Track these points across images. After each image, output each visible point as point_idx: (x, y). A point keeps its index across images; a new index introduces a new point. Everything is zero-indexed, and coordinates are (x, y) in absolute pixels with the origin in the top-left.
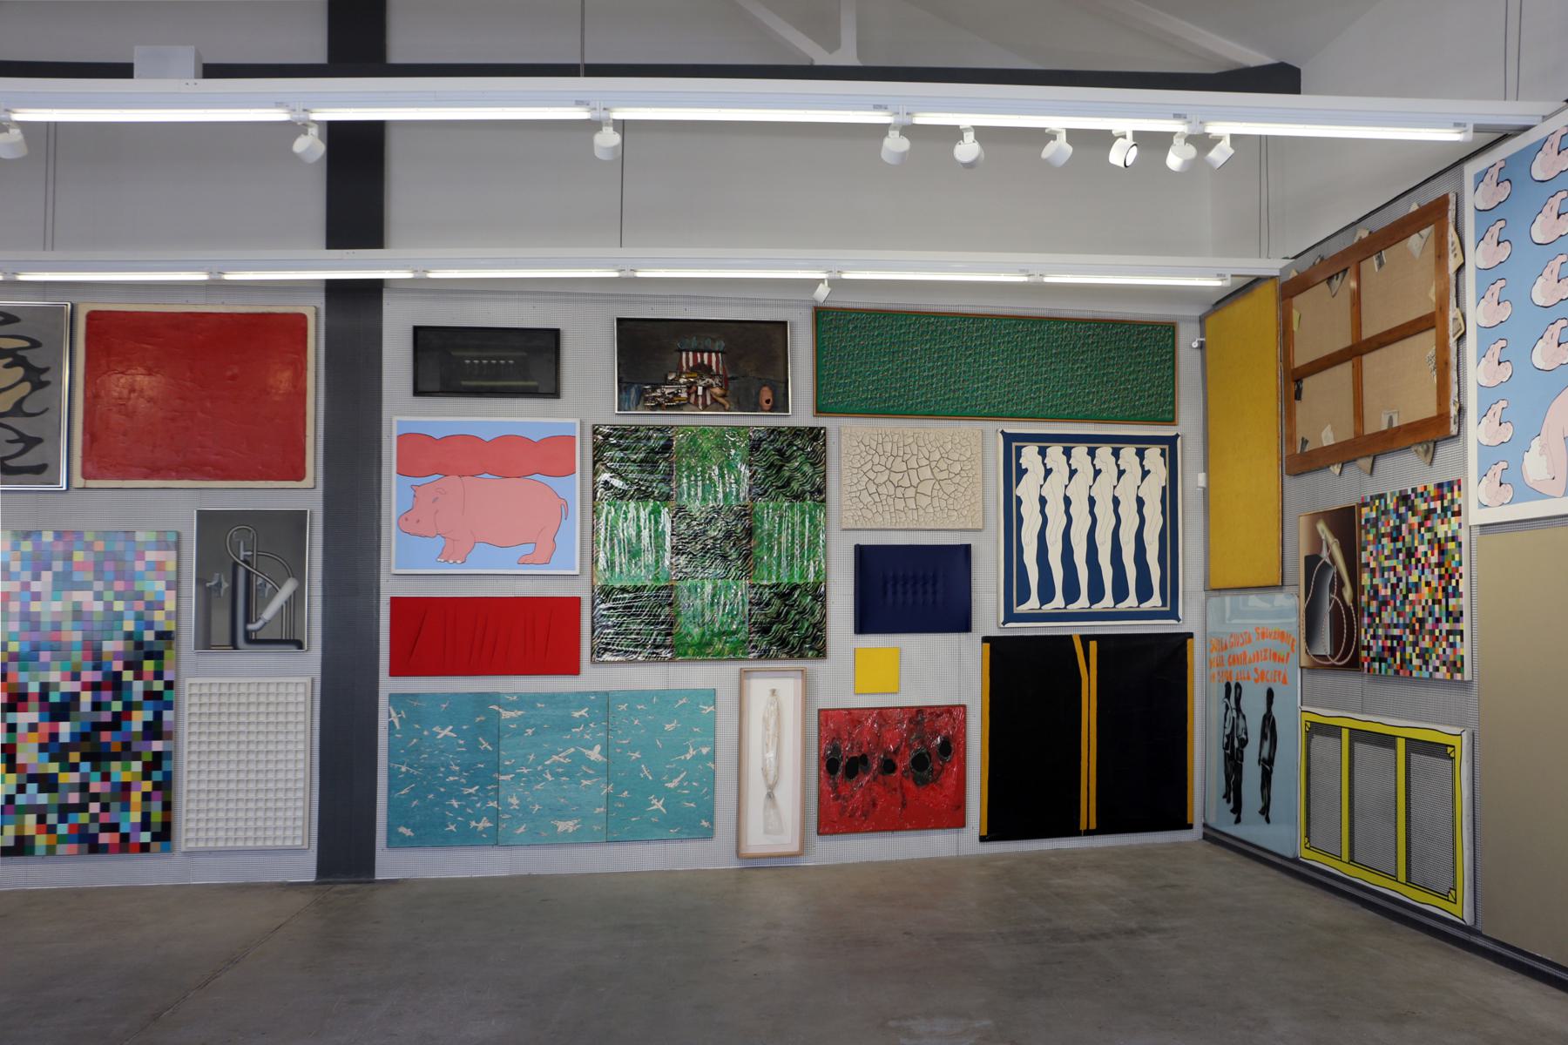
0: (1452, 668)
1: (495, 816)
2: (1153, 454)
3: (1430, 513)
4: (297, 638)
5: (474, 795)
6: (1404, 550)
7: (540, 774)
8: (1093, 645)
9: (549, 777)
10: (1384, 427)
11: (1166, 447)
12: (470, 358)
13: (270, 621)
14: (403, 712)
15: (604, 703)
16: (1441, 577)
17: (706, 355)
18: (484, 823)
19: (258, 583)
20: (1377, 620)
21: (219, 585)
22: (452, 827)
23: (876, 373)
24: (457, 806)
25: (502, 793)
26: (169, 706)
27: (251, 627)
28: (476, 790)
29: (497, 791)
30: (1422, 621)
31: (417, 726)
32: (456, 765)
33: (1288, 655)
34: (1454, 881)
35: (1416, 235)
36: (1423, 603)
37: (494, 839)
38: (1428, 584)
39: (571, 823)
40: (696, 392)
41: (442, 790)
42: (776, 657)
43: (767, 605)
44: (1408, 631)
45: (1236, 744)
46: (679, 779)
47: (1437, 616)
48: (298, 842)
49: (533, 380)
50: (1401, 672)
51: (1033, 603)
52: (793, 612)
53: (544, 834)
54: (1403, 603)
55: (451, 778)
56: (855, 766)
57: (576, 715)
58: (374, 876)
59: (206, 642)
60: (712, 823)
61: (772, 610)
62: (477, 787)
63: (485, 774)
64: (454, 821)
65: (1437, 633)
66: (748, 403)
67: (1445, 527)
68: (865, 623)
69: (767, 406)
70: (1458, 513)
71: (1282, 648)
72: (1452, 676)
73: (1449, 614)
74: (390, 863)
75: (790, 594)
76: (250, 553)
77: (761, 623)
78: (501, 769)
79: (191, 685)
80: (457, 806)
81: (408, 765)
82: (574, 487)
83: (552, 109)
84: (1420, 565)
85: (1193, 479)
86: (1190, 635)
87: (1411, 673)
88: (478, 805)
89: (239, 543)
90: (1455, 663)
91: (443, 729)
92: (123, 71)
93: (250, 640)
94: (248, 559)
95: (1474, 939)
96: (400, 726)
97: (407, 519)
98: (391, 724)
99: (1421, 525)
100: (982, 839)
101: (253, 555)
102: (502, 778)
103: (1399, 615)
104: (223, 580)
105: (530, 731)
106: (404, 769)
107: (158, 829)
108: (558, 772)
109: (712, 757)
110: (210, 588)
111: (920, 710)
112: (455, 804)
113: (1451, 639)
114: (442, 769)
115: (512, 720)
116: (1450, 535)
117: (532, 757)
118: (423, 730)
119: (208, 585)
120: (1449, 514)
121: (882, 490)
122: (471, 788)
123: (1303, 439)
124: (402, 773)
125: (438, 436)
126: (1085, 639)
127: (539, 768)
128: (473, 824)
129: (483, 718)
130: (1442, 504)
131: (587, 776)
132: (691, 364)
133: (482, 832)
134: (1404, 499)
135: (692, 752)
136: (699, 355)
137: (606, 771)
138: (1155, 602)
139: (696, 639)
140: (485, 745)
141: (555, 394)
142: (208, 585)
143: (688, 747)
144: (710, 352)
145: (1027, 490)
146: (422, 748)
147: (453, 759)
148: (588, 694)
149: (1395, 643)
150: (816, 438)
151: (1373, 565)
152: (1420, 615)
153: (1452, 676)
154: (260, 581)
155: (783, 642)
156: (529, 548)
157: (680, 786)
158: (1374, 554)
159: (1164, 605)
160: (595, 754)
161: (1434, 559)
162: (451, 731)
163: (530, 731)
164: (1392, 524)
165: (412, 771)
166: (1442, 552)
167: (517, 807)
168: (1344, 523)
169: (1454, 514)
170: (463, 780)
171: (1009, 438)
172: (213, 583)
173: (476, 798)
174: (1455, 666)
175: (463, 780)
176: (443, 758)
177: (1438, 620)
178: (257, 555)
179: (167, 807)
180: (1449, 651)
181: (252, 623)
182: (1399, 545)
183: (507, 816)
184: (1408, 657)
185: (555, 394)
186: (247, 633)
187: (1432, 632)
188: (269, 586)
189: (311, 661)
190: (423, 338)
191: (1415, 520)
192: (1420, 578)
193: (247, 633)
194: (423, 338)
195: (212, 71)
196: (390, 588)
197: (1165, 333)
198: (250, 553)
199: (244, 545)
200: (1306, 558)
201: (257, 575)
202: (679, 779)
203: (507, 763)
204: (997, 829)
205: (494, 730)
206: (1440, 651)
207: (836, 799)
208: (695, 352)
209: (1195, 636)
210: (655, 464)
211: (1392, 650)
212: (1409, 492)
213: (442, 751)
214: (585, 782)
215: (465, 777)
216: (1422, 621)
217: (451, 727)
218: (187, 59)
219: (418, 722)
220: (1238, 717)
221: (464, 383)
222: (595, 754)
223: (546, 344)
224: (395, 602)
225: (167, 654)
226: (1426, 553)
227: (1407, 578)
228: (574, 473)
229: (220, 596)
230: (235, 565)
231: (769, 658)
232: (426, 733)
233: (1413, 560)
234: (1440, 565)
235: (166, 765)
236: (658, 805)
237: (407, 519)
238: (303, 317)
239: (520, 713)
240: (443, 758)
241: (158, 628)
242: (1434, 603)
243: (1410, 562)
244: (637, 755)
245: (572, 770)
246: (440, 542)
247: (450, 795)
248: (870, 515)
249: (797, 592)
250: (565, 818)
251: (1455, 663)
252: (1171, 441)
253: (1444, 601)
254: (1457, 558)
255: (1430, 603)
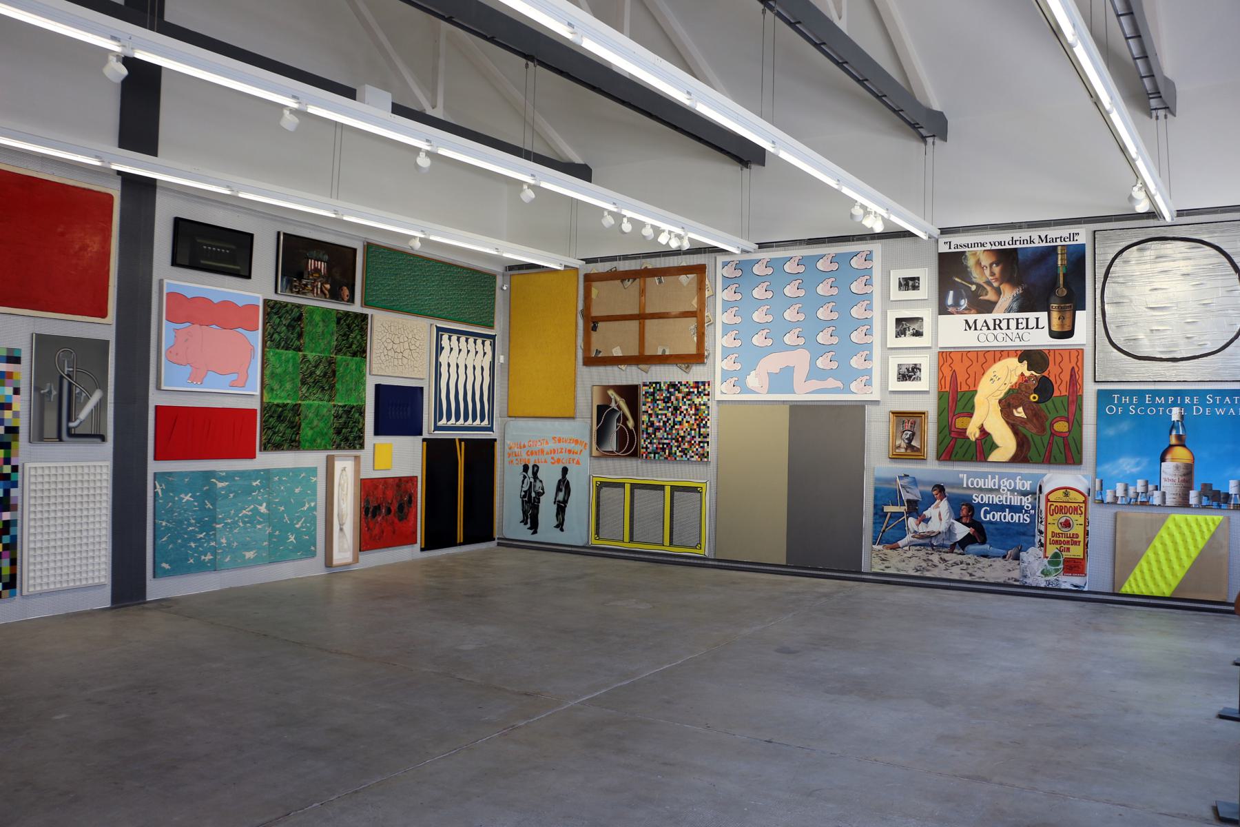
0: (701, 457)
1: (214, 551)
2: (488, 343)
3: (689, 393)
4: (101, 433)
5: (203, 539)
6: (672, 407)
7: (235, 523)
8: (463, 443)
9: (241, 524)
10: (660, 353)
11: (492, 340)
12: (208, 245)
13: (84, 420)
14: (163, 485)
15: (267, 475)
16: (696, 420)
17: (319, 263)
18: (209, 557)
19: (77, 392)
20: (653, 436)
21: (50, 392)
22: (192, 561)
23: (389, 285)
24: (194, 547)
25: (218, 536)
26: (15, 485)
27: (72, 425)
28: (204, 535)
29: (214, 534)
30: (683, 438)
31: (171, 494)
32: (193, 519)
33: (581, 451)
34: (700, 540)
35: (684, 276)
36: (684, 430)
37: (214, 567)
38: (688, 422)
39: (252, 553)
40: (317, 286)
41: (186, 536)
42: (344, 449)
43: (341, 417)
44: (674, 441)
45: (533, 495)
46: (301, 522)
47: (693, 435)
48: (103, 580)
49: (238, 266)
50: (669, 458)
51: (444, 422)
52: (351, 422)
53: (239, 561)
54: (671, 429)
55: (191, 528)
56: (377, 509)
57: (254, 484)
58: (145, 599)
59: (39, 436)
60: (316, 548)
61: (341, 421)
62: (204, 533)
63: (208, 524)
64: (192, 556)
65: (693, 442)
66: (335, 295)
67: (700, 400)
68: (378, 432)
69: (346, 298)
70: (708, 395)
71: (577, 448)
72: (701, 460)
73: (700, 435)
74: (156, 589)
75: (350, 412)
76: (71, 369)
77: (338, 428)
78: (217, 521)
79: (30, 468)
80: (194, 547)
81: (168, 521)
82: (257, 337)
83: (339, 115)
84: (683, 414)
85: (501, 359)
86: (495, 440)
87: (675, 459)
88: (205, 545)
89: (64, 361)
90: (703, 454)
91: (186, 496)
92: (350, 93)
93: (71, 434)
94: (71, 374)
95: (707, 562)
96: (162, 494)
97: (170, 352)
98: (155, 494)
99: (683, 398)
100: (422, 550)
101: (73, 371)
102: (218, 526)
103: (668, 434)
104: (53, 389)
105: (232, 495)
106: (164, 524)
107: (7, 580)
108: (245, 521)
109: (315, 508)
110: (43, 394)
111: (400, 479)
112: (193, 545)
113: (701, 445)
114: (186, 523)
115: (223, 488)
116: (702, 403)
117: (233, 512)
118: (175, 497)
119: (42, 392)
120: (702, 395)
121: (390, 353)
122: (201, 533)
123: (597, 350)
124: (162, 526)
125: (189, 297)
126: (461, 440)
127: (237, 519)
128: (203, 557)
129: (207, 488)
130: (698, 390)
131: (260, 523)
132: (313, 268)
133: (208, 562)
134: (673, 385)
135: (307, 505)
136: (316, 262)
137: (268, 518)
138: (486, 422)
139: (309, 438)
140: (209, 506)
141: (248, 276)
142: (42, 392)
143: (305, 502)
144: (321, 261)
145: (443, 359)
146: (175, 509)
147: (192, 515)
148: (260, 471)
149: (665, 446)
150: (363, 321)
151: (650, 412)
152: (682, 434)
153: (701, 460)
154: (78, 391)
155: (347, 439)
156: (234, 377)
157: (302, 527)
158: (652, 407)
159: (489, 424)
160: (263, 509)
161: (692, 412)
162: (190, 497)
163: (232, 495)
164: (664, 395)
165: (169, 524)
166: (697, 409)
167: (225, 545)
168: (630, 393)
169: (705, 395)
170: (197, 529)
171: (439, 329)
172: (46, 391)
173: (204, 540)
174: (704, 456)
175: (197, 529)
176: (186, 515)
177: (694, 437)
178: (77, 371)
179: (13, 562)
180: (699, 449)
181: (72, 422)
182: (670, 405)
183: (220, 551)
184: (673, 452)
185: (248, 276)
186: (69, 429)
187: (689, 442)
188: (84, 394)
189: (109, 446)
190: (180, 225)
191: (680, 395)
192: (683, 419)
193: (69, 429)
194: (180, 225)
195: (398, 109)
196: (156, 399)
197: (492, 277)
198: (71, 369)
199: (68, 363)
200: (598, 406)
201: (76, 386)
202: (301, 522)
203: (220, 516)
204: (429, 545)
205: (211, 495)
206: (695, 450)
207: (368, 530)
208: (315, 260)
209: (21, 431)
210: (294, 328)
211: (663, 449)
212: (677, 383)
213: (185, 511)
214: (259, 527)
215: (198, 527)
216: (683, 438)
217: (190, 494)
218: (387, 99)
219: (172, 492)
220: (535, 481)
221: (202, 262)
222: (263, 509)
223: (245, 241)
224: (157, 408)
225: (13, 444)
226: (687, 410)
227: (674, 419)
228: (258, 329)
229: (50, 401)
230: (62, 378)
231: (341, 449)
232: (176, 499)
233: (678, 412)
234: (695, 415)
235: (12, 530)
236: (292, 538)
237: (170, 352)
238: (110, 197)
239: (227, 483)
240: (186, 515)
241: (7, 424)
242: (691, 430)
243: (676, 412)
244: (282, 508)
245: (251, 520)
246: (188, 369)
247: (190, 540)
248: (383, 367)
249: (353, 410)
250: (249, 550)
251: (703, 454)
252: (493, 337)
253: (697, 430)
254: (706, 412)
255: (689, 430)
